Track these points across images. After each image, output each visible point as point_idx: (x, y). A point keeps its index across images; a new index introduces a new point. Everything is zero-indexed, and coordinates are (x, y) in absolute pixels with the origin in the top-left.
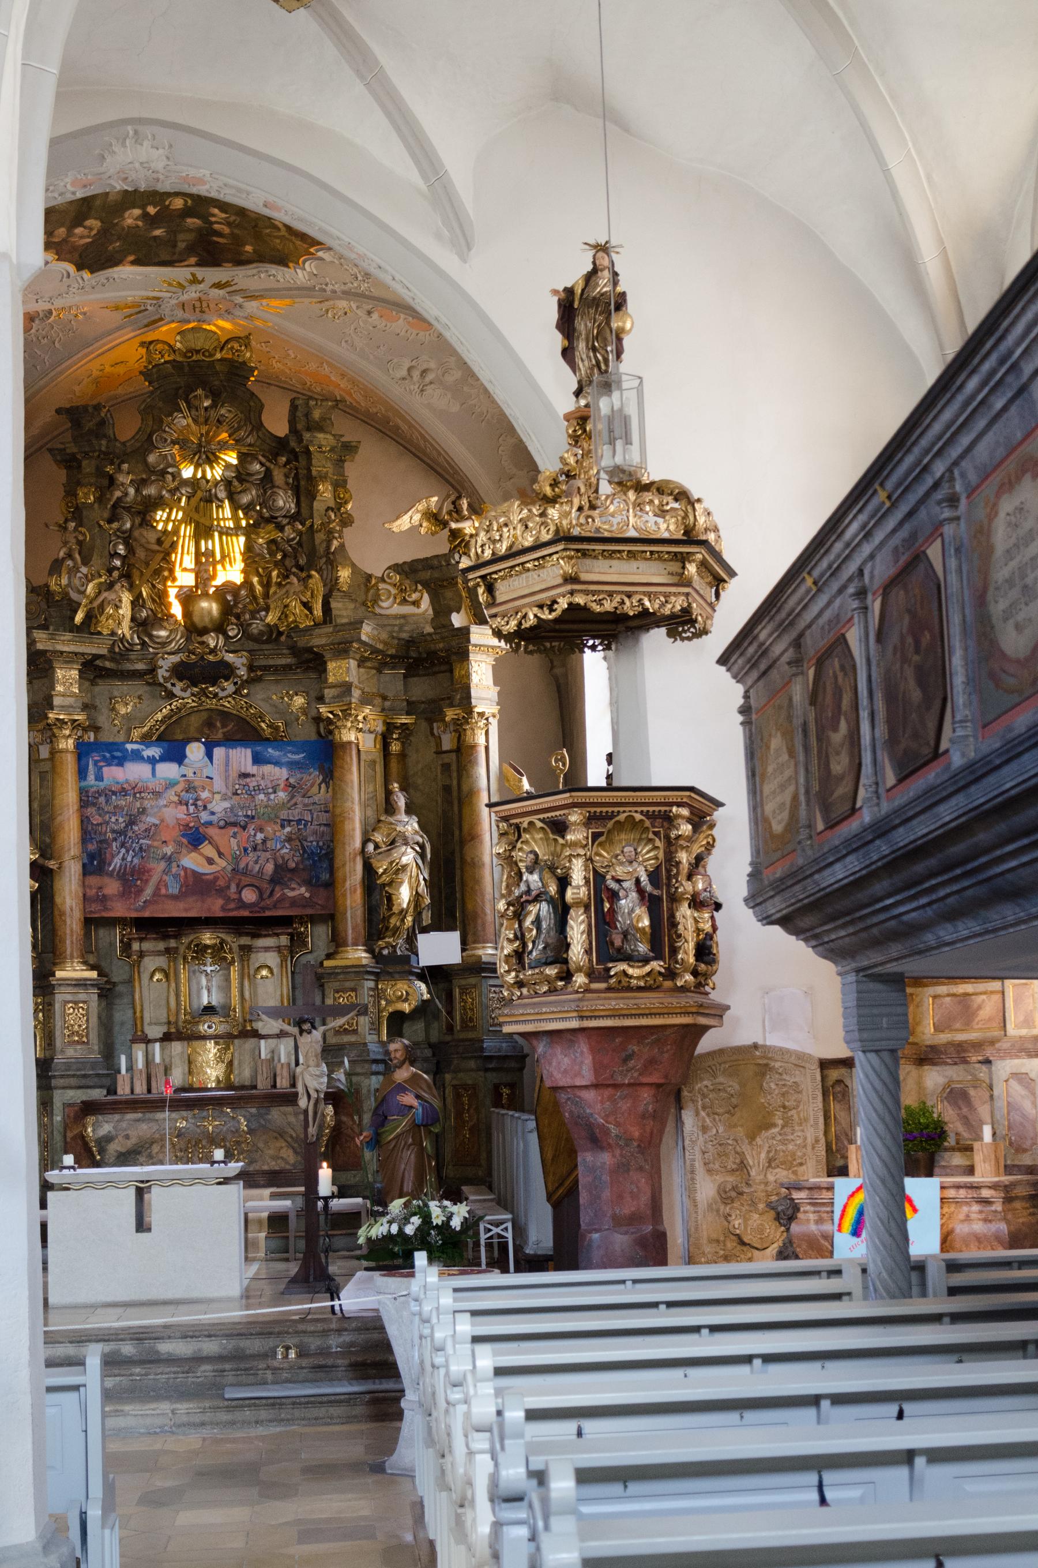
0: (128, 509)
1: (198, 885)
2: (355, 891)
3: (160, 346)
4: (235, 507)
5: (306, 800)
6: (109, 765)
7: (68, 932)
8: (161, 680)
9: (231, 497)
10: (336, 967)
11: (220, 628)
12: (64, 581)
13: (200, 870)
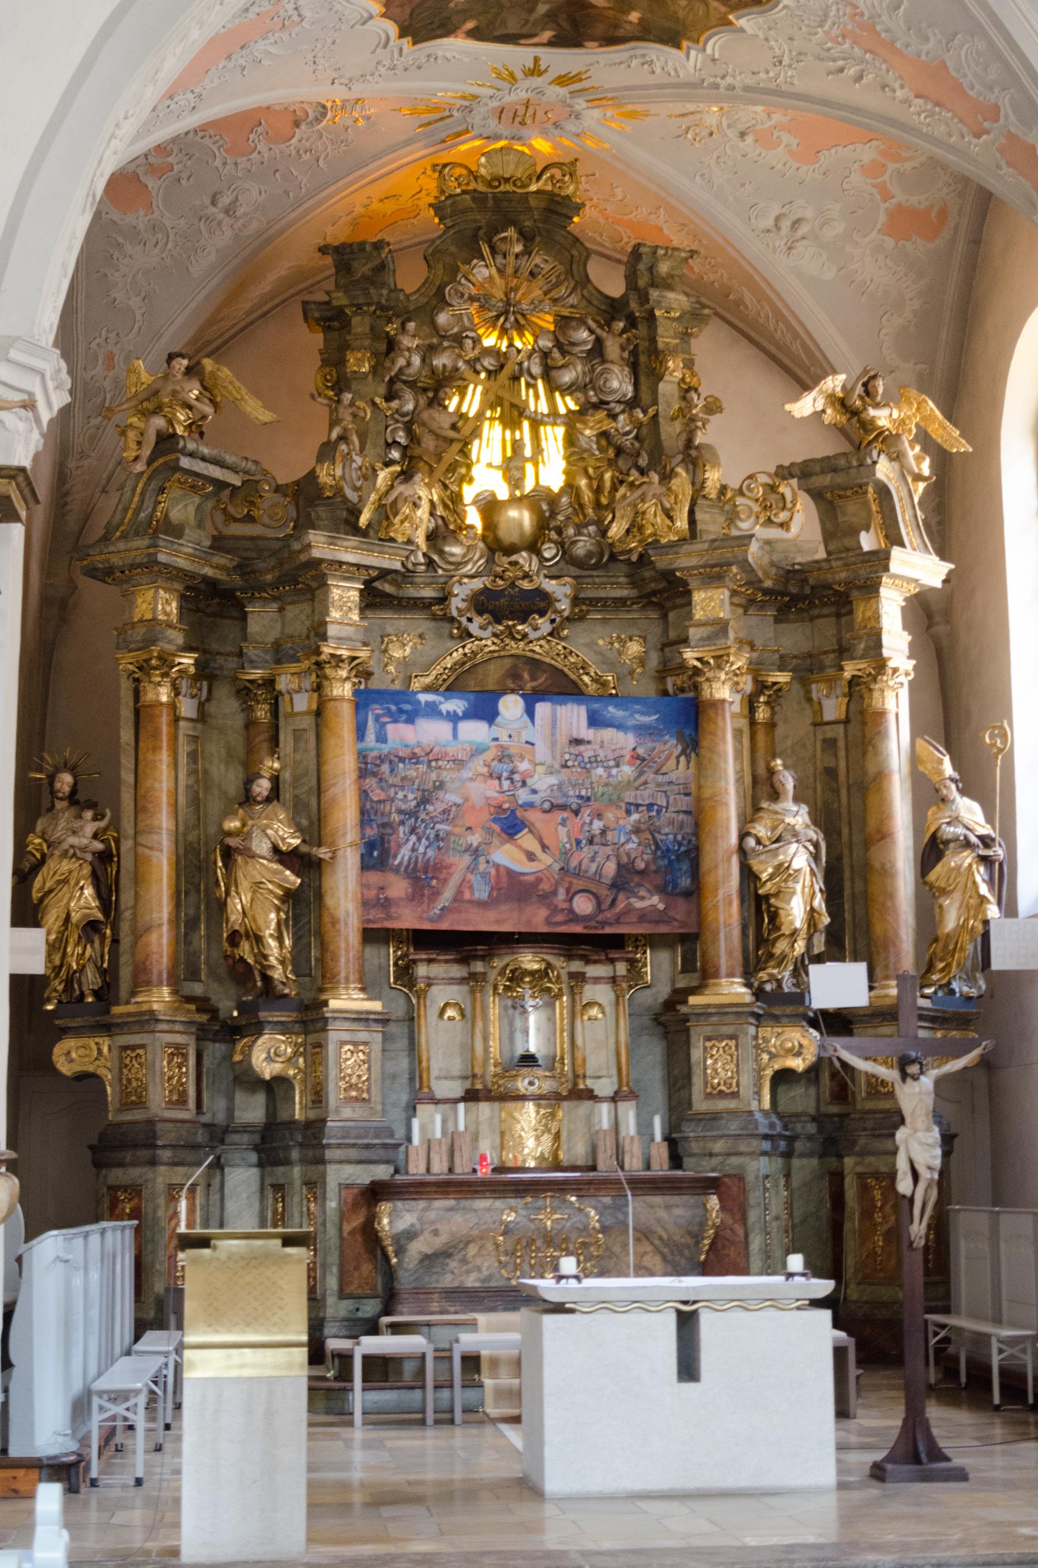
0: (412, 384)
1: (514, 888)
2: (730, 903)
3: (458, 171)
4: (552, 387)
5: (660, 778)
6: (395, 721)
7: (343, 945)
8: (455, 613)
9: (547, 374)
10: (709, 1006)
11: (533, 547)
12: (339, 472)
13: (517, 868)
